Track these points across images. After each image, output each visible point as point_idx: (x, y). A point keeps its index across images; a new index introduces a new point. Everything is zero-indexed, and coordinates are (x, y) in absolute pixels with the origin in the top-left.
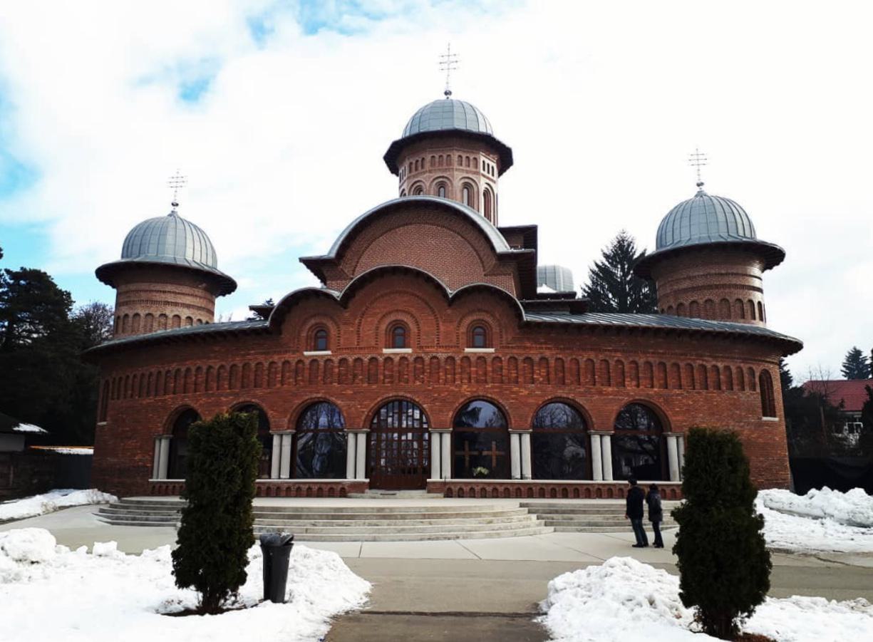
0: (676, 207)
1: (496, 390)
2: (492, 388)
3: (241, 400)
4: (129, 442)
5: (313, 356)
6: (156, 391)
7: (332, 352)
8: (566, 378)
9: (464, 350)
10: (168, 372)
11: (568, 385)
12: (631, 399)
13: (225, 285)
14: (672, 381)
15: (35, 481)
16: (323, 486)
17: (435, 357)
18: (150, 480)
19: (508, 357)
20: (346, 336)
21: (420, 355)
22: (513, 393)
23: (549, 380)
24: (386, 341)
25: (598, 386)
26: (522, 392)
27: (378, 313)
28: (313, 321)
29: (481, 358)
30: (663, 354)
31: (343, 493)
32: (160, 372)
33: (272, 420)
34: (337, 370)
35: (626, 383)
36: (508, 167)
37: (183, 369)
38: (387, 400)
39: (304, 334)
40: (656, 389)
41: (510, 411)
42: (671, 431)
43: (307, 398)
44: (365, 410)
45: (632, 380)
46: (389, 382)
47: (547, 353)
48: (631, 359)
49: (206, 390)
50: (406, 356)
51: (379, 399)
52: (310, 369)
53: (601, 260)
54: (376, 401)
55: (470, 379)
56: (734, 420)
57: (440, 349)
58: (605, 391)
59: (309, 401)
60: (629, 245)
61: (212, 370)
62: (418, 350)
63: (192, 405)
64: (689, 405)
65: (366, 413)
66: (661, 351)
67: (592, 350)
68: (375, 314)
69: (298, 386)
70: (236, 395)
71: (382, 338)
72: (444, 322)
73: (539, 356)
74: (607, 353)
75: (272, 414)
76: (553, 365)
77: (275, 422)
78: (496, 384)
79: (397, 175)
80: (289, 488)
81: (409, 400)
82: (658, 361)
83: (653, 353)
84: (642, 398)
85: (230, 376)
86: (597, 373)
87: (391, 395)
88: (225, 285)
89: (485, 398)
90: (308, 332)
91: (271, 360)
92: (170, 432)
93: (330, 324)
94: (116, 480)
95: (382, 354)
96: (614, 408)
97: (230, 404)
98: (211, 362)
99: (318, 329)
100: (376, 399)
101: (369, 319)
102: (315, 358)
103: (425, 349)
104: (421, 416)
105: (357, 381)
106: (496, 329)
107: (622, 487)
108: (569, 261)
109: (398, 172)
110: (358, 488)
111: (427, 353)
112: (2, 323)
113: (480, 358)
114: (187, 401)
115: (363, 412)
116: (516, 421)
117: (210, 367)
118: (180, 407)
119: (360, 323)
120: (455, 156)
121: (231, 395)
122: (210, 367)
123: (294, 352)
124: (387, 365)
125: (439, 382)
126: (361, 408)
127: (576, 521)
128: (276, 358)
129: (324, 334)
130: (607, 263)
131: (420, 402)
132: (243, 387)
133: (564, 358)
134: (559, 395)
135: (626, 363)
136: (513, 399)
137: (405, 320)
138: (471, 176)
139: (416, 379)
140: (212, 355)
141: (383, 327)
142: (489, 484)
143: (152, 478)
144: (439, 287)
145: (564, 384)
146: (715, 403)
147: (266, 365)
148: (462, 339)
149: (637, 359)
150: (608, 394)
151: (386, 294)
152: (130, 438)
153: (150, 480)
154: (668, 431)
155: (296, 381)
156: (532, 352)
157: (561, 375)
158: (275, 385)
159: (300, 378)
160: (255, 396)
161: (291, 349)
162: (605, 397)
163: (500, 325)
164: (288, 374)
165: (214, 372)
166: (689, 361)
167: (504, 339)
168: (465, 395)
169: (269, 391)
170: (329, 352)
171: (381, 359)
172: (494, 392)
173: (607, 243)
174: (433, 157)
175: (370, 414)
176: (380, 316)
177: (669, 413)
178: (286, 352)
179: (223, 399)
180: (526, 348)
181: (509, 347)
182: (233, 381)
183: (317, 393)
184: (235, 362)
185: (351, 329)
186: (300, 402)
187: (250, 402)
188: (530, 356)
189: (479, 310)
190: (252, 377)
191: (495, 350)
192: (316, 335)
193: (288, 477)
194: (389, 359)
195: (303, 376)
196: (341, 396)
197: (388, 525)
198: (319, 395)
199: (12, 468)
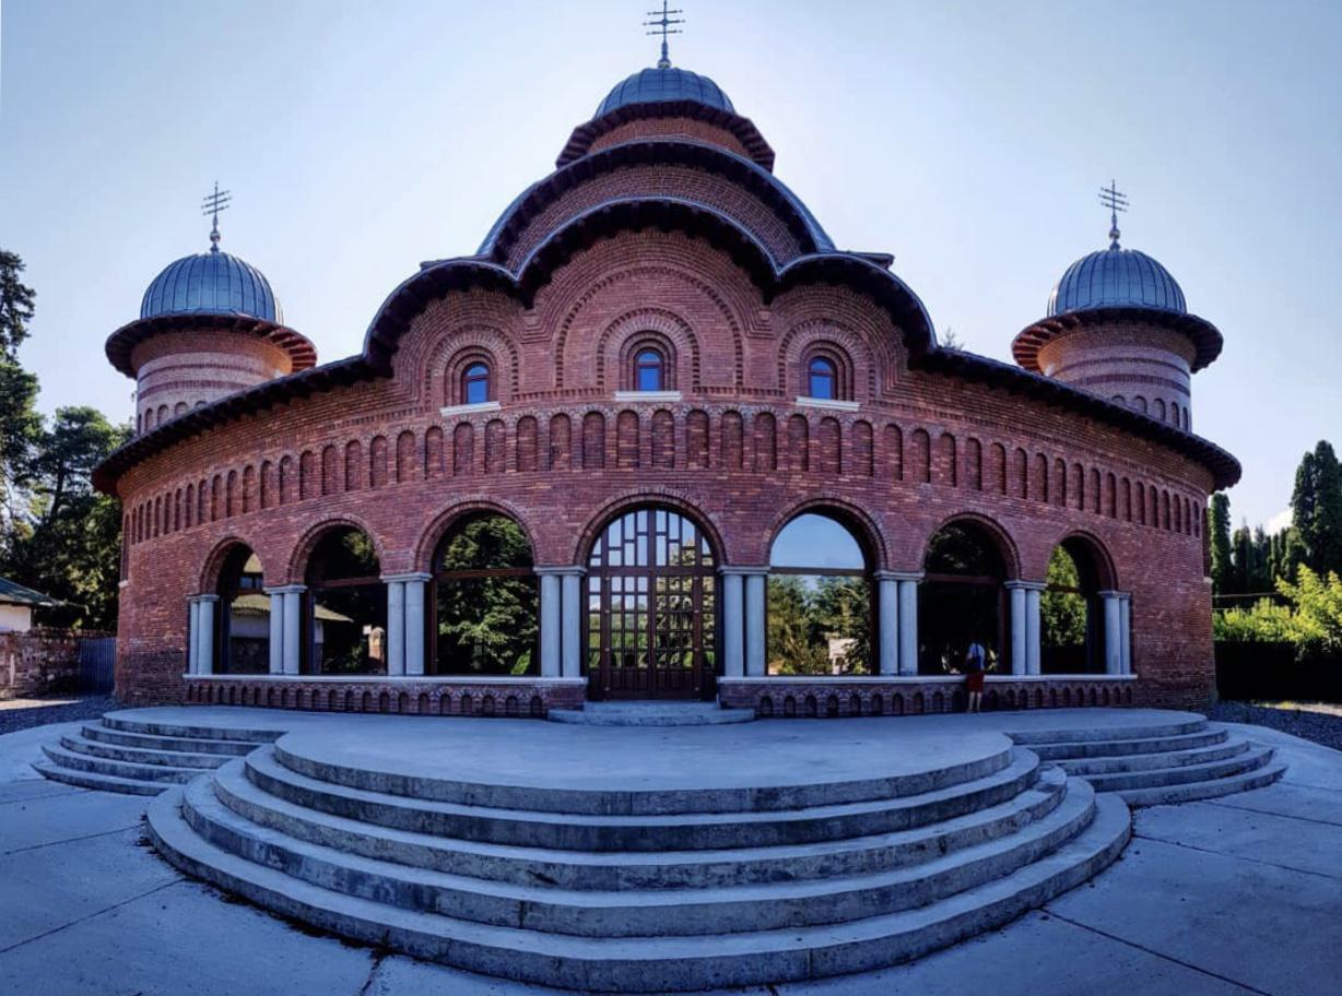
2: (853, 483)
4: (155, 612)
6: (188, 518)
7: (501, 404)
8: (983, 478)
9: (795, 400)
10: (203, 482)
11: (988, 491)
15: (51, 677)
17: (734, 413)
18: (186, 676)
19: (885, 423)
21: (699, 406)
23: (954, 477)
24: (621, 376)
25: (1030, 499)
26: (908, 497)
27: (603, 317)
28: (456, 345)
29: (830, 420)
30: (1113, 459)
32: (190, 486)
34: (512, 442)
35: (1068, 501)
37: (224, 474)
38: (626, 502)
39: (438, 373)
40: (1102, 517)
42: (1116, 589)
44: (578, 524)
46: (630, 465)
47: (955, 427)
49: (263, 507)
50: (669, 408)
51: (608, 501)
52: (455, 443)
54: (602, 506)
55: (805, 463)
57: (746, 396)
63: (241, 536)
65: (580, 531)
66: (1111, 455)
67: (1024, 432)
68: (594, 320)
69: (430, 480)
70: (316, 508)
71: (613, 369)
72: (755, 337)
73: (941, 429)
75: (382, 541)
76: (963, 451)
77: (388, 556)
78: (859, 477)
80: (424, 696)
83: (1102, 456)
84: (1086, 529)
85: (301, 475)
86: (1029, 477)
87: (634, 491)
90: (446, 370)
91: (374, 434)
92: (214, 588)
93: (496, 346)
95: (612, 405)
98: (268, 454)
99: (468, 361)
101: (582, 331)
102: (464, 419)
103: (709, 393)
104: (698, 542)
105: (558, 464)
106: (861, 366)
107: (1055, 685)
111: (714, 402)
113: (826, 419)
114: (235, 530)
115: (574, 530)
118: (223, 541)
119: (563, 339)
121: (304, 510)
122: (266, 463)
123: (421, 411)
124: (624, 428)
125: (741, 467)
127: (1134, 774)
128: (383, 428)
129: (481, 371)
131: (702, 508)
132: (324, 492)
133: (980, 440)
134: (971, 508)
136: (893, 509)
139: (689, 459)
140: (268, 440)
141: (615, 344)
142: (1072, 682)
143: (187, 672)
145: (980, 488)
147: (366, 443)
148: (792, 376)
150: (1043, 516)
151: (620, 276)
153: (186, 676)
154: (1110, 589)
155: (427, 471)
156: (927, 420)
158: (386, 482)
159: (435, 465)
160: (348, 509)
161: (414, 405)
162: (1041, 521)
163: (870, 357)
164: (409, 459)
167: (878, 387)
169: (373, 494)
170: (494, 406)
171: (611, 416)
172: (856, 494)
175: (589, 533)
176: (606, 322)
177: (1116, 559)
179: (292, 520)
180: (917, 409)
182: (307, 484)
183: (471, 492)
184: (307, 447)
186: (437, 512)
188: (924, 427)
189: (826, 321)
190: (341, 473)
191: (861, 406)
192: (464, 373)
193: (421, 672)
194: (628, 413)
196: (523, 493)
198: (478, 497)
199: (12, 657)
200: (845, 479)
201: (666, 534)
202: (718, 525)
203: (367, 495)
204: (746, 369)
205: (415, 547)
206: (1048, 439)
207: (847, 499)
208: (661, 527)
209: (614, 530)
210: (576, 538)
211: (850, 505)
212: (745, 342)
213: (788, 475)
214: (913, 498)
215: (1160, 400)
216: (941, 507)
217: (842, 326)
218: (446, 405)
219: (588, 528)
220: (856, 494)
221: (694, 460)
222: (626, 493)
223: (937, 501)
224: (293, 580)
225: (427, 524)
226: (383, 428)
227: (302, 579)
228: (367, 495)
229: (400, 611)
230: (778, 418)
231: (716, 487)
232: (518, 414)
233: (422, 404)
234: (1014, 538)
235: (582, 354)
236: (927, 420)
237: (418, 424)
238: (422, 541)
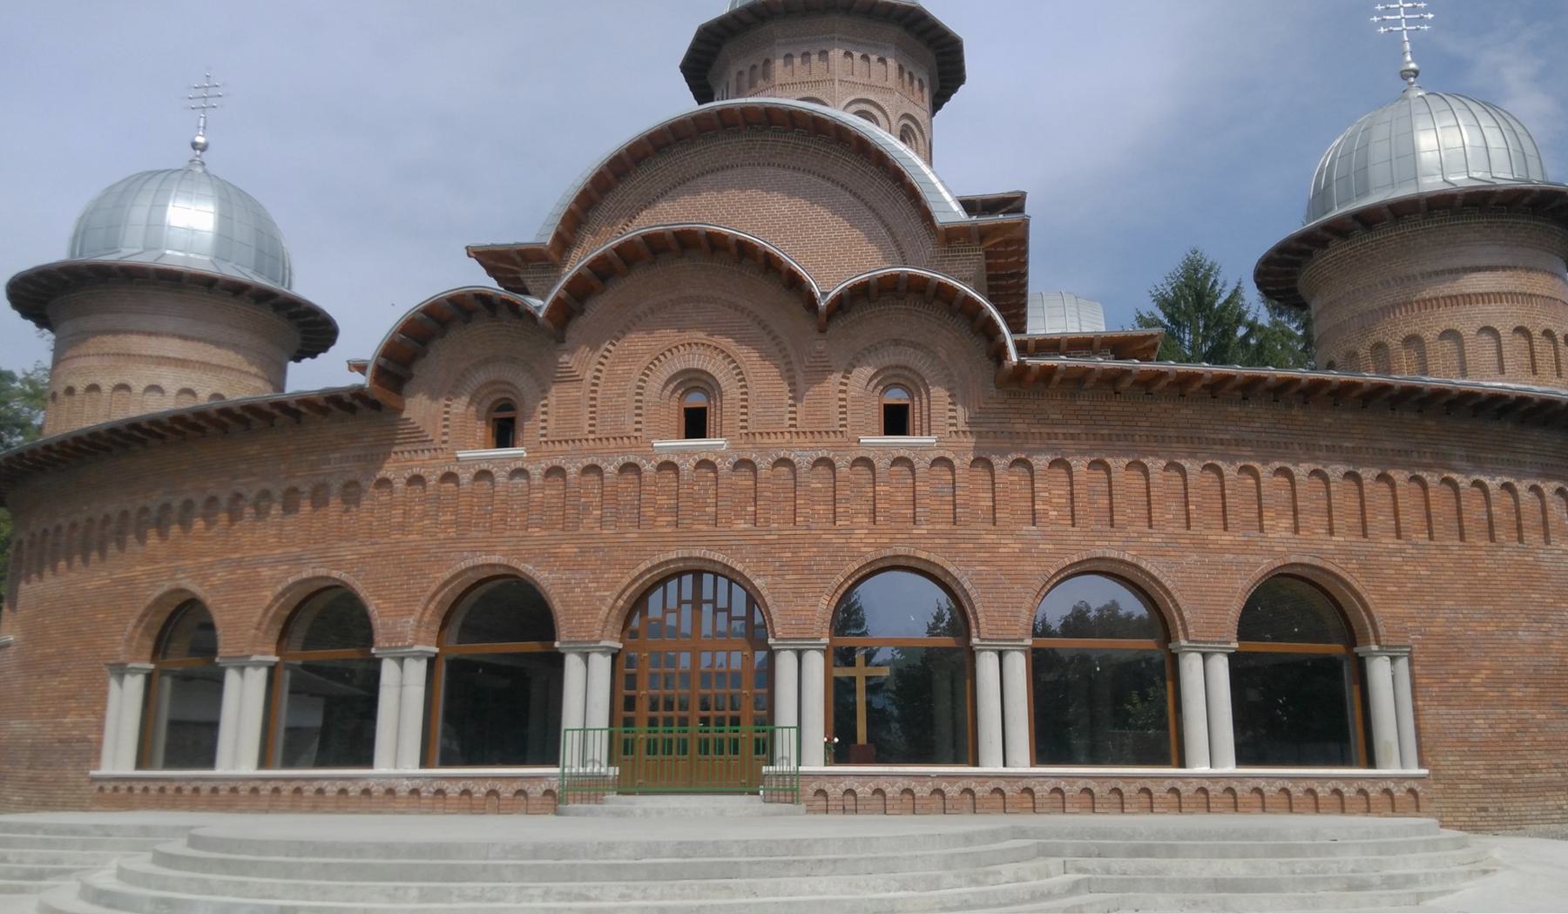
2: (932, 534)
3: (305, 575)
10: (144, 510)
11: (1123, 527)
12: (1278, 563)
14: (1380, 520)
16: (500, 786)
21: (746, 456)
22: (982, 547)
25: (1196, 528)
31: (554, 800)
33: (377, 622)
36: (955, 90)
37: (177, 503)
43: (463, 565)
45: (1279, 515)
46: (669, 524)
58: (1215, 542)
59: (470, 574)
60: (1206, 277)
64: (1419, 578)
65: (610, 601)
70: (297, 561)
81: (718, 568)
84: (1306, 560)
94: (24, 774)
97: (279, 582)
102: (484, 466)
110: (589, 789)
111: (763, 450)
115: (603, 599)
120: (836, 54)
134: (1099, 553)
136: (983, 562)
137: (710, 369)
138: (871, 97)
144: (794, 283)
150: (1223, 550)
152: (55, 673)
168: (862, 555)
176: (647, 359)
177: (1370, 598)
179: (266, 572)
183: (488, 553)
186: (447, 575)
187: (327, 578)
189: (897, 342)
195: (456, 513)
197: (623, 897)
198: (495, 559)
200: (922, 530)
201: (714, 601)
202: (764, 592)
203: (365, 550)
205: (418, 615)
206: (1222, 442)
208: (707, 593)
209: (655, 599)
210: (605, 609)
211: (926, 561)
213: (850, 531)
214: (1011, 546)
215: (1488, 330)
217: (914, 345)
219: (619, 597)
222: (662, 558)
225: (433, 588)
227: (273, 648)
230: (838, 464)
231: (763, 549)
234: (1168, 584)
235: (619, 395)
238: (426, 608)
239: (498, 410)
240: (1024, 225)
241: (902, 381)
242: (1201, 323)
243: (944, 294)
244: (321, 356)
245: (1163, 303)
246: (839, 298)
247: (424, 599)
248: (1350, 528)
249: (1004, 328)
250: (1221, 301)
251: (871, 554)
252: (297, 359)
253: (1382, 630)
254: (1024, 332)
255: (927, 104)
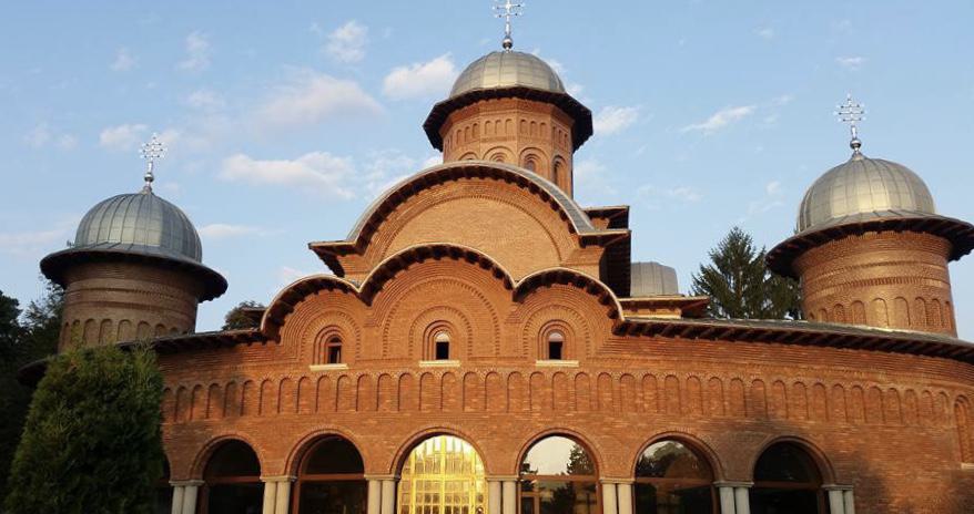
0: (803, 203)
1: (580, 420)
5: (322, 371)
12: (777, 436)
13: (213, 285)
20: (368, 344)
22: (605, 424)
38: (398, 458)
41: (602, 451)
47: (654, 369)
48: (775, 379)
50: (453, 371)
53: (710, 263)
56: (923, 467)
57: (499, 362)
60: (744, 244)
61: (185, 392)
62: (470, 363)
65: (395, 452)
74: (740, 369)
79: (441, 150)
82: (814, 381)
88: (213, 285)
89: (566, 432)
95: (418, 369)
96: (754, 448)
100: (410, 432)
108: (675, 252)
109: (442, 143)
111: (481, 367)
112: (184, 502)
115: (390, 451)
116: (610, 466)
117: (182, 388)
126: (388, 445)
130: (715, 267)
135: (768, 384)
136: (607, 434)
146: (895, 443)
149: (783, 378)
154: (830, 483)
157: (675, 400)
165: (187, 393)
166: (858, 383)
169: (260, 420)
173: (716, 241)
174: (488, 122)
177: (601, 473)
178: (286, 365)
181: (597, 359)
184: (216, 381)
185: (375, 333)
188: (627, 372)
189: (556, 306)
194: (426, 374)
198: (330, 426)
203: (254, 420)
204: (502, 344)
207: (572, 428)
212: (502, 327)
216: (646, 430)
218: (313, 363)
220: (578, 424)
221: (468, 405)
223: (644, 425)
224: (194, 476)
225: (296, 442)
226: (271, 375)
227: (200, 476)
228: (254, 420)
229: (273, 502)
232: (358, 373)
233: (298, 360)
236: (631, 367)
237: (295, 374)
239: (332, 341)
240: (630, 232)
241: (559, 328)
242: (741, 273)
243: (581, 282)
244: (215, 300)
245: (717, 260)
246: (524, 284)
247: (290, 449)
248: (820, 416)
249: (612, 293)
250: (753, 259)
251: (542, 427)
252: (201, 302)
253: (837, 475)
254: (628, 296)
255: (570, 147)
